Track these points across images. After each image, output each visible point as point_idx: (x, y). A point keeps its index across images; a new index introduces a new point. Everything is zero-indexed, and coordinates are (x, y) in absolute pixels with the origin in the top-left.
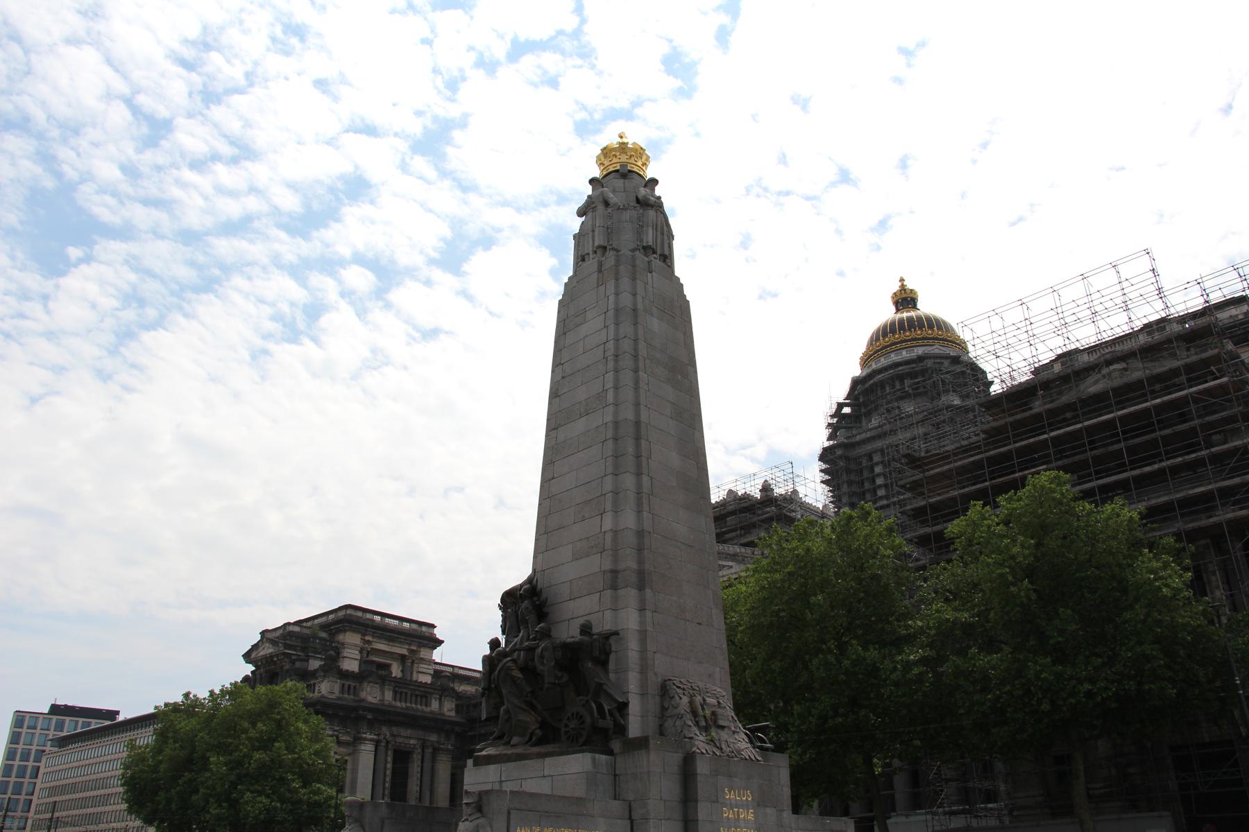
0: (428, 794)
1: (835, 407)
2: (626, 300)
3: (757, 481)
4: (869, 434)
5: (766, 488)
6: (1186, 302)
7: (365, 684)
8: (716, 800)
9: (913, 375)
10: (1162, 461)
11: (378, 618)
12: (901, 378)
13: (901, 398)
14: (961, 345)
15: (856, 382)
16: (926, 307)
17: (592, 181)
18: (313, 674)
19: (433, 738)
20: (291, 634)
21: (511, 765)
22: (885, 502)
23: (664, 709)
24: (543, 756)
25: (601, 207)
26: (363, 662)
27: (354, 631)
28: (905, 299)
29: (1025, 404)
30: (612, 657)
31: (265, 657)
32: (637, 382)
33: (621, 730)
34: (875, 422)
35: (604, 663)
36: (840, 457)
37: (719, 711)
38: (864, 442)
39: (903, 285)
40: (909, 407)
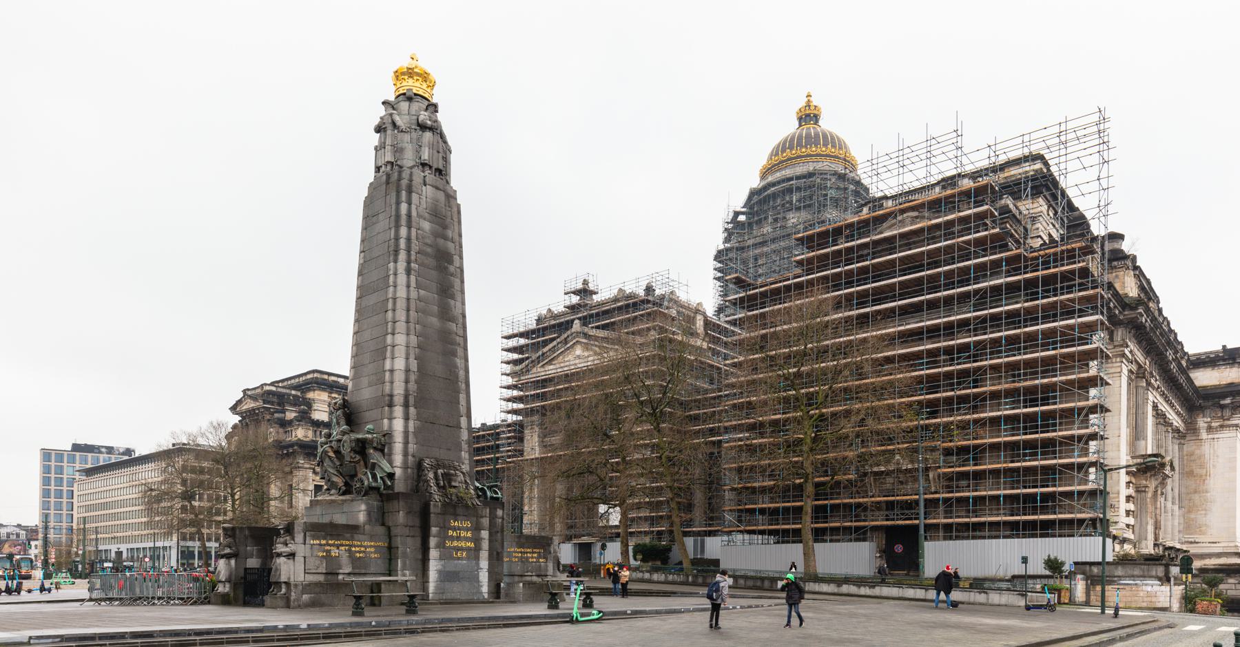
5: (649, 289)
8: (445, 528)
12: (790, 191)
14: (849, 163)
15: (753, 193)
16: (826, 124)
18: (290, 423)
20: (269, 392)
23: (419, 476)
27: (324, 390)
28: (809, 116)
34: (767, 229)
39: (808, 105)
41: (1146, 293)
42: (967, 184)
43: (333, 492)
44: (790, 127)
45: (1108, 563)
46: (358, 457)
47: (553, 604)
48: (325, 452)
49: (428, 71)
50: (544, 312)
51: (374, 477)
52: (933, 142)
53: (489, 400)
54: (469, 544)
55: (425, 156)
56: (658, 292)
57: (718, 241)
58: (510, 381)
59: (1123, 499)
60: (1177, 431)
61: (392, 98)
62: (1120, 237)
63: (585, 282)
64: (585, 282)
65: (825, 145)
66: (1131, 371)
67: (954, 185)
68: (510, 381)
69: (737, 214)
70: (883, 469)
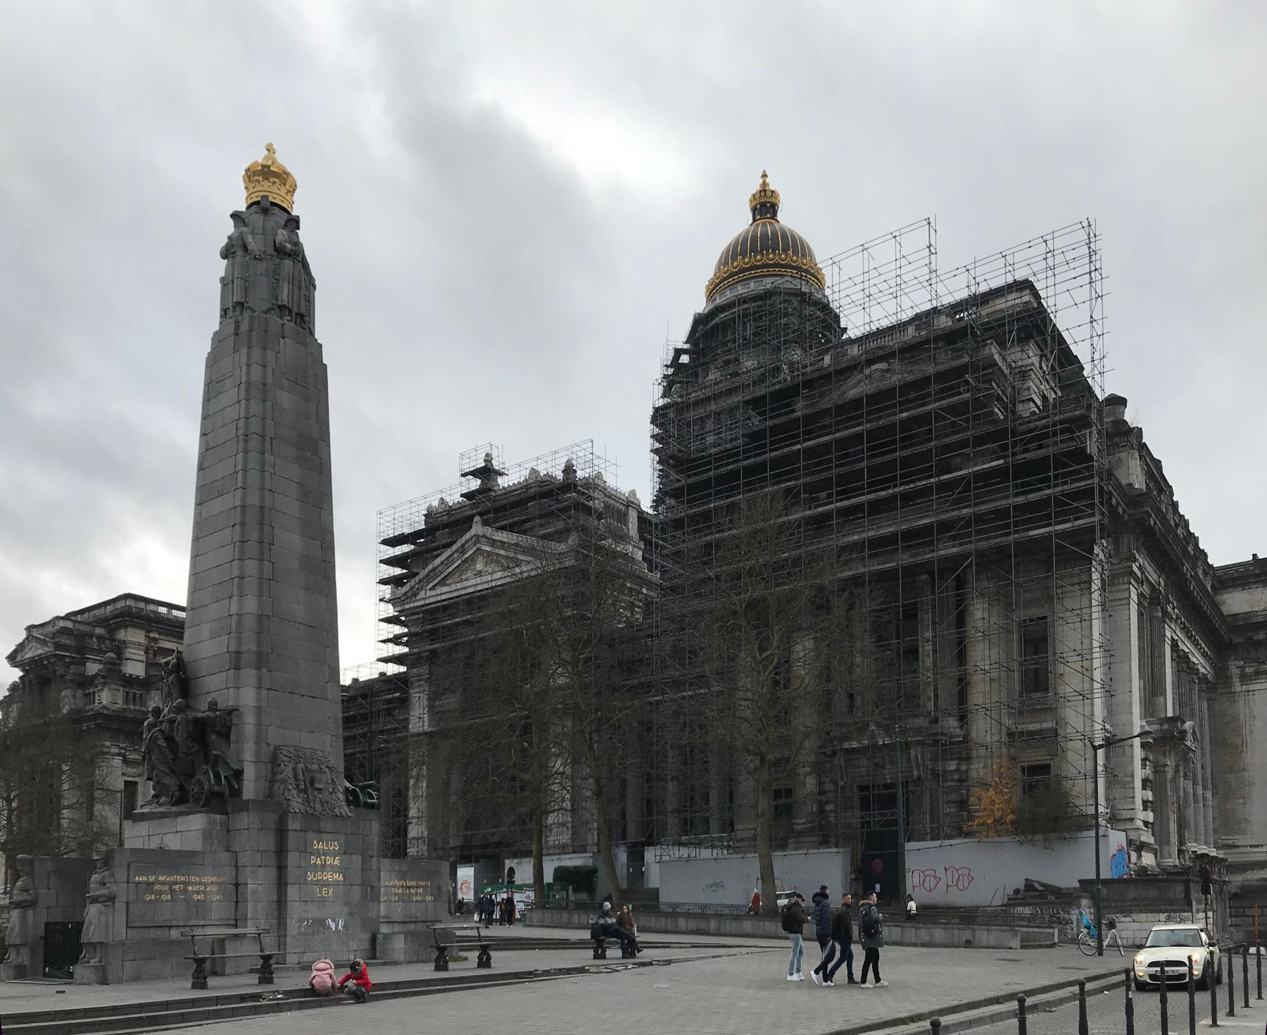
1: (671, 354)
2: (256, 372)
3: (558, 461)
5: (569, 470)
6: (954, 291)
7: (153, 692)
8: (306, 850)
10: (896, 486)
11: (163, 610)
15: (699, 321)
17: (235, 216)
20: (64, 631)
21: (155, 822)
24: (180, 814)
25: (240, 253)
26: (149, 665)
28: (765, 206)
29: (788, 405)
30: (234, 729)
31: (32, 660)
32: (263, 464)
33: (237, 793)
34: (713, 376)
35: (227, 736)
37: (317, 775)
39: (764, 184)
41: (1156, 482)
42: (944, 322)
43: (163, 799)
44: (741, 222)
45: (1105, 882)
46: (196, 748)
47: (441, 965)
48: (153, 740)
49: (289, 169)
50: (436, 503)
51: (217, 777)
52: (904, 261)
53: (364, 642)
54: (336, 876)
55: (284, 297)
56: (580, 474)
57: (653, 397)
58: (390, 611)
59: (1138, 784)
60: (1204, 679)
61: (242, 207)
62: (1122, 402)
63: (488, 459)
64: (488, 459)
65: (785, 250)
66: (1140, 595)
67: (929, 324)
68: (390, 611)
69: (678, 352)
70: (855, 745)
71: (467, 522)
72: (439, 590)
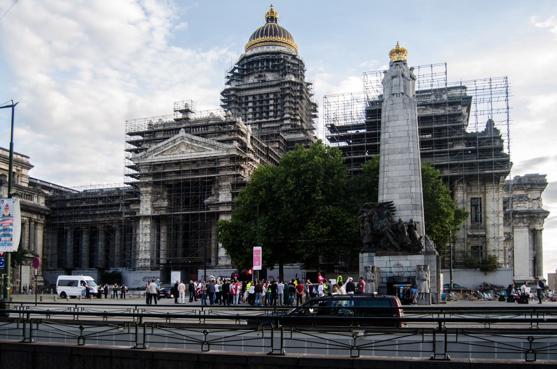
0: (33, 245)
4: (248, 86)
9: (273, 60)
12: (268, 60)
13: (267, 71)
19: (35, 217)
22: (272, 119)
28: (271, 18)
36: (233, 95)
38: (243, 90)
40: (270, 77)
71: (177, 130)
72: (160, 157)
